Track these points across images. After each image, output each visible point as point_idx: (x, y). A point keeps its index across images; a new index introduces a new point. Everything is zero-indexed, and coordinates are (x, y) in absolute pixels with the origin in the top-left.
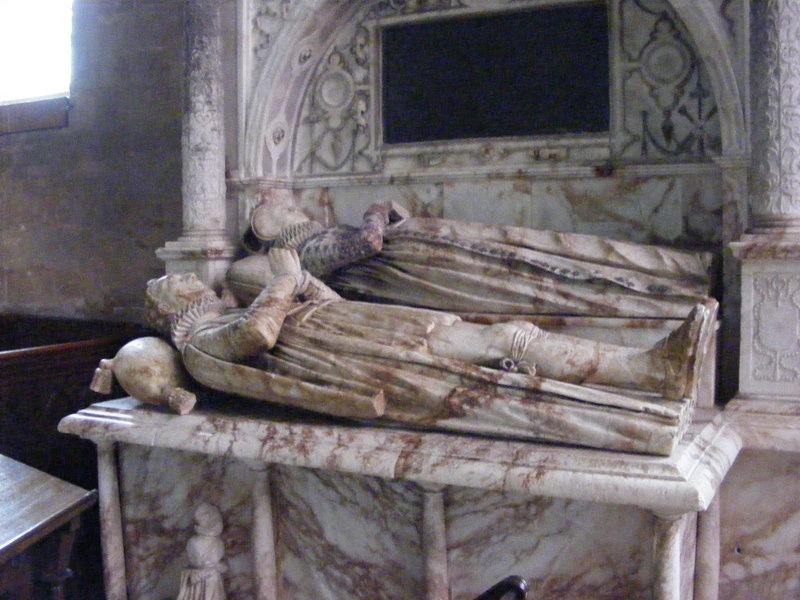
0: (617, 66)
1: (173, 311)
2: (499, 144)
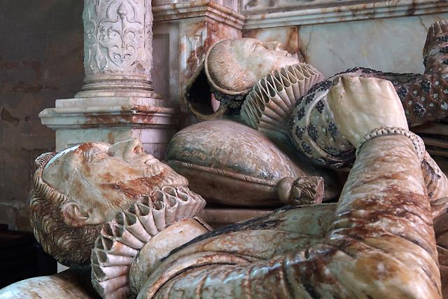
1: (96, 219)
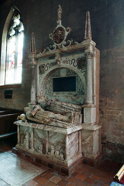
0: (77, 84)
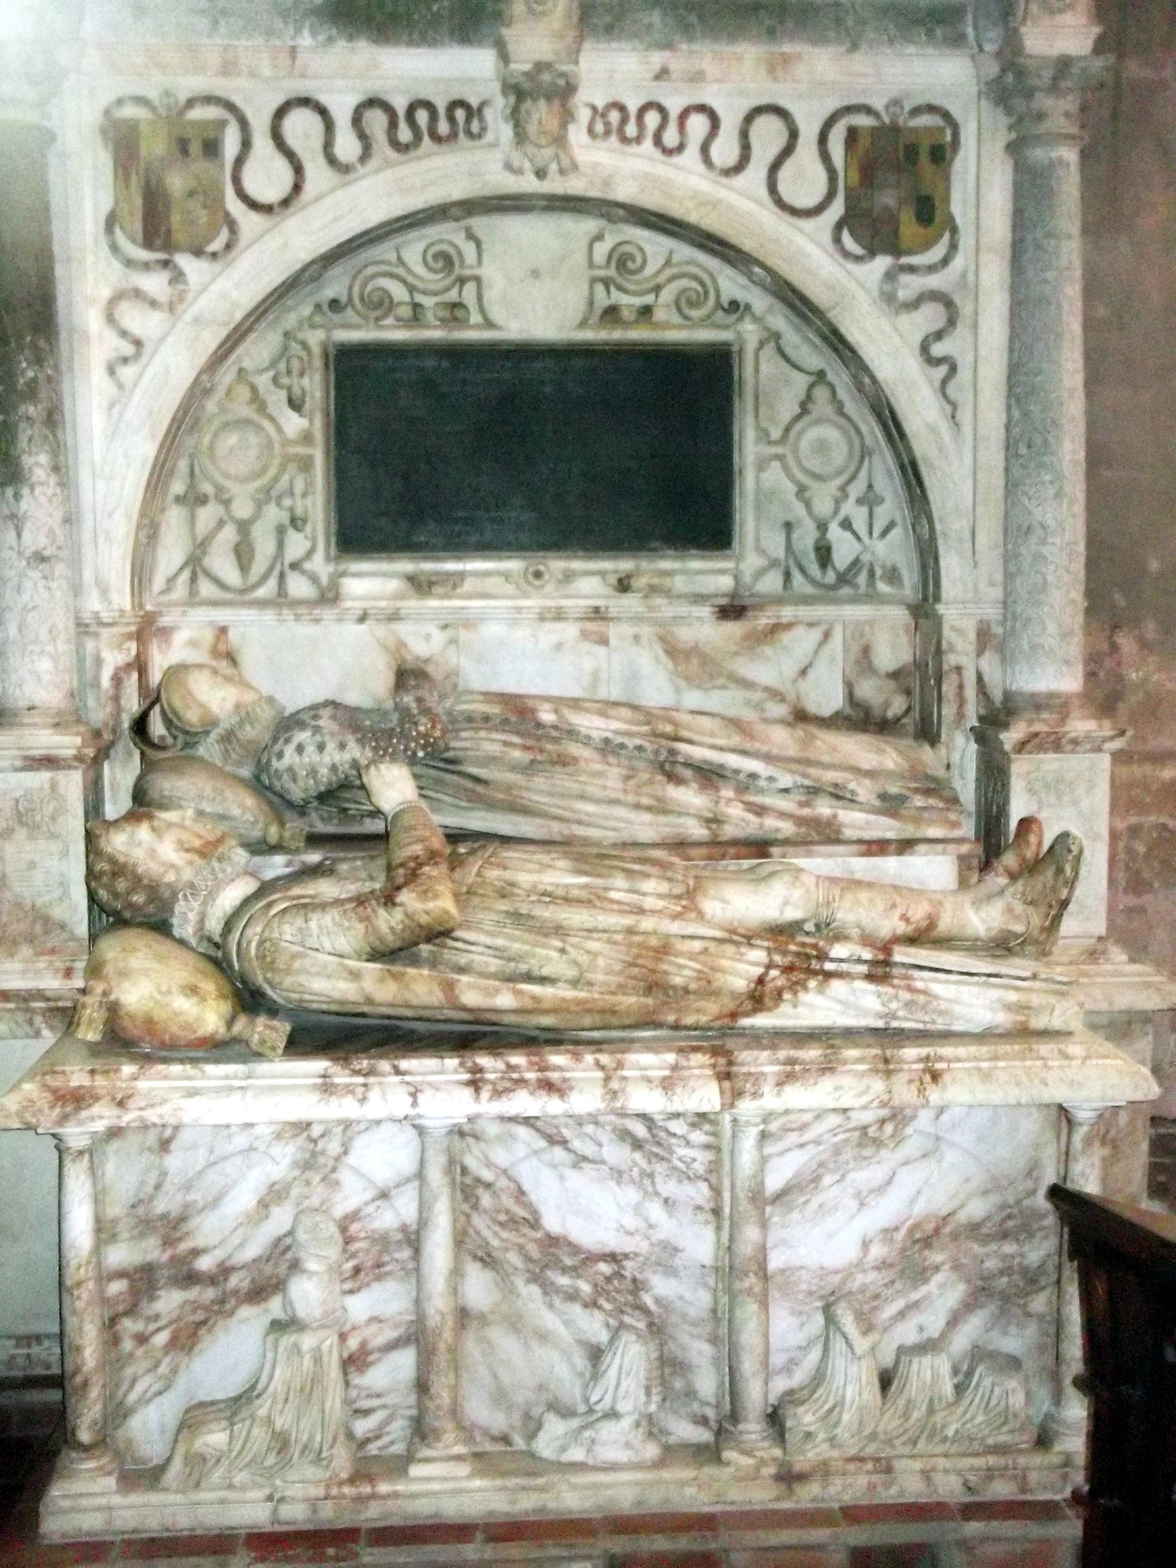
0: (749, 448)
2: (557, 564)
